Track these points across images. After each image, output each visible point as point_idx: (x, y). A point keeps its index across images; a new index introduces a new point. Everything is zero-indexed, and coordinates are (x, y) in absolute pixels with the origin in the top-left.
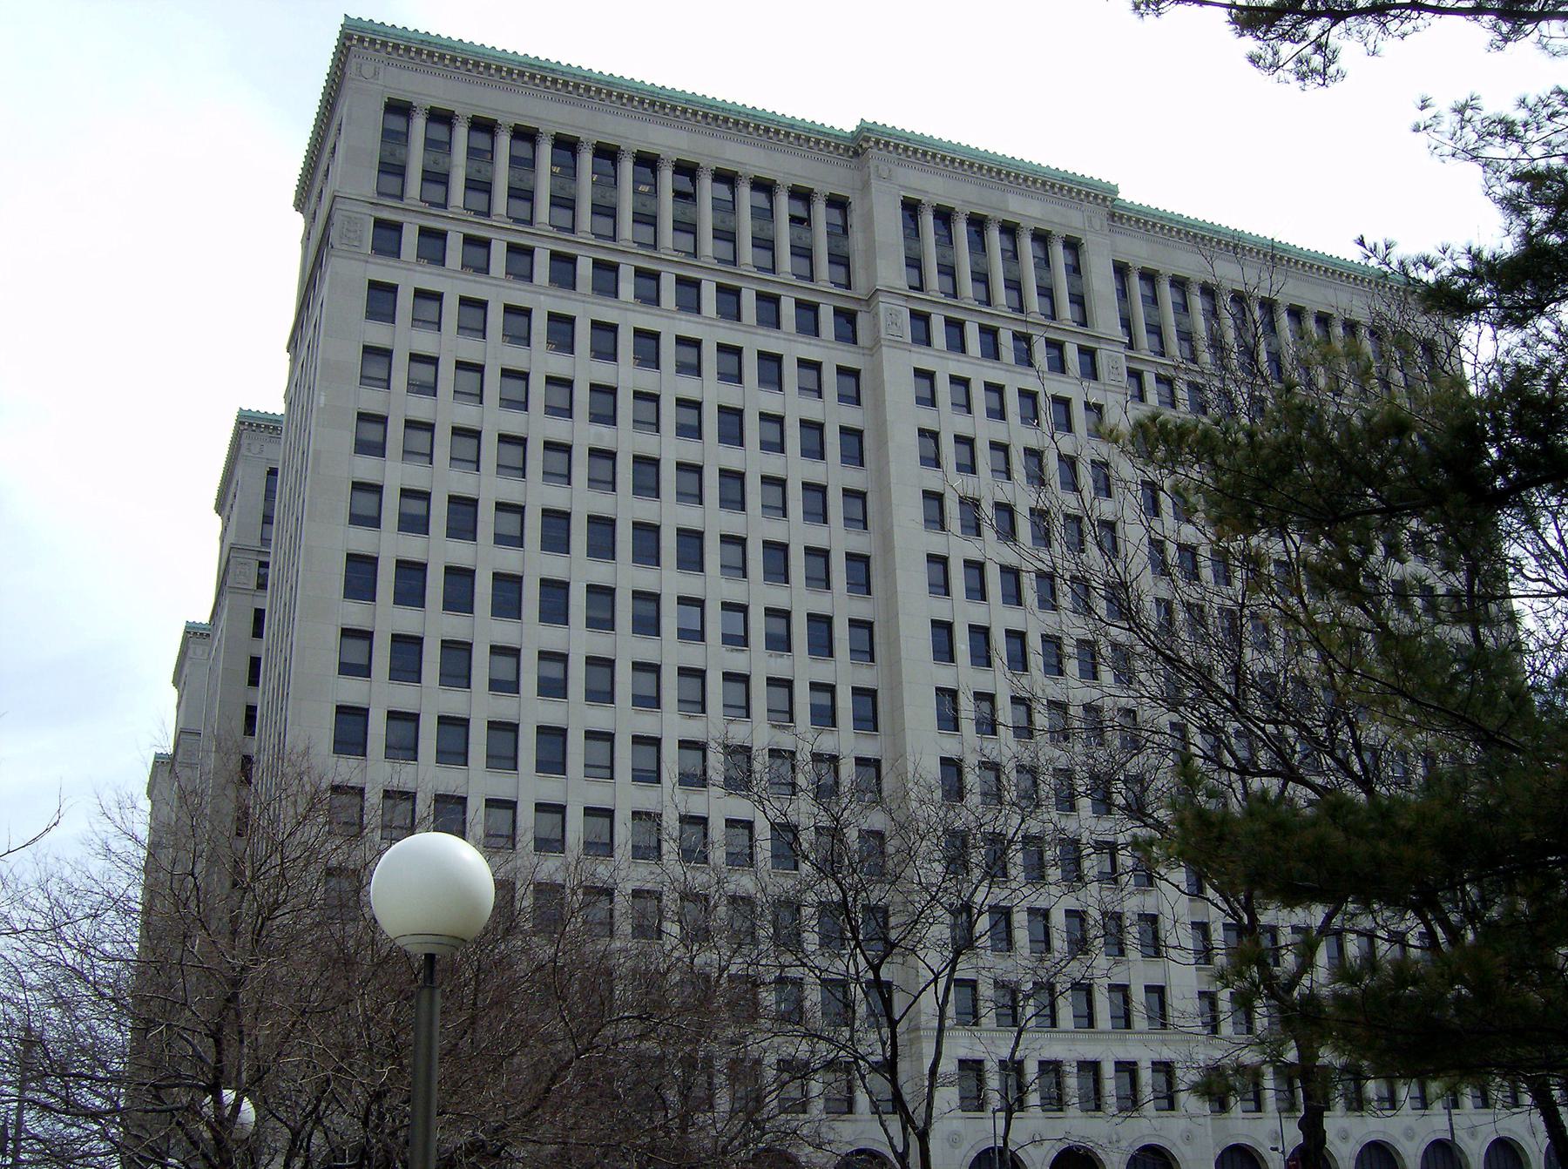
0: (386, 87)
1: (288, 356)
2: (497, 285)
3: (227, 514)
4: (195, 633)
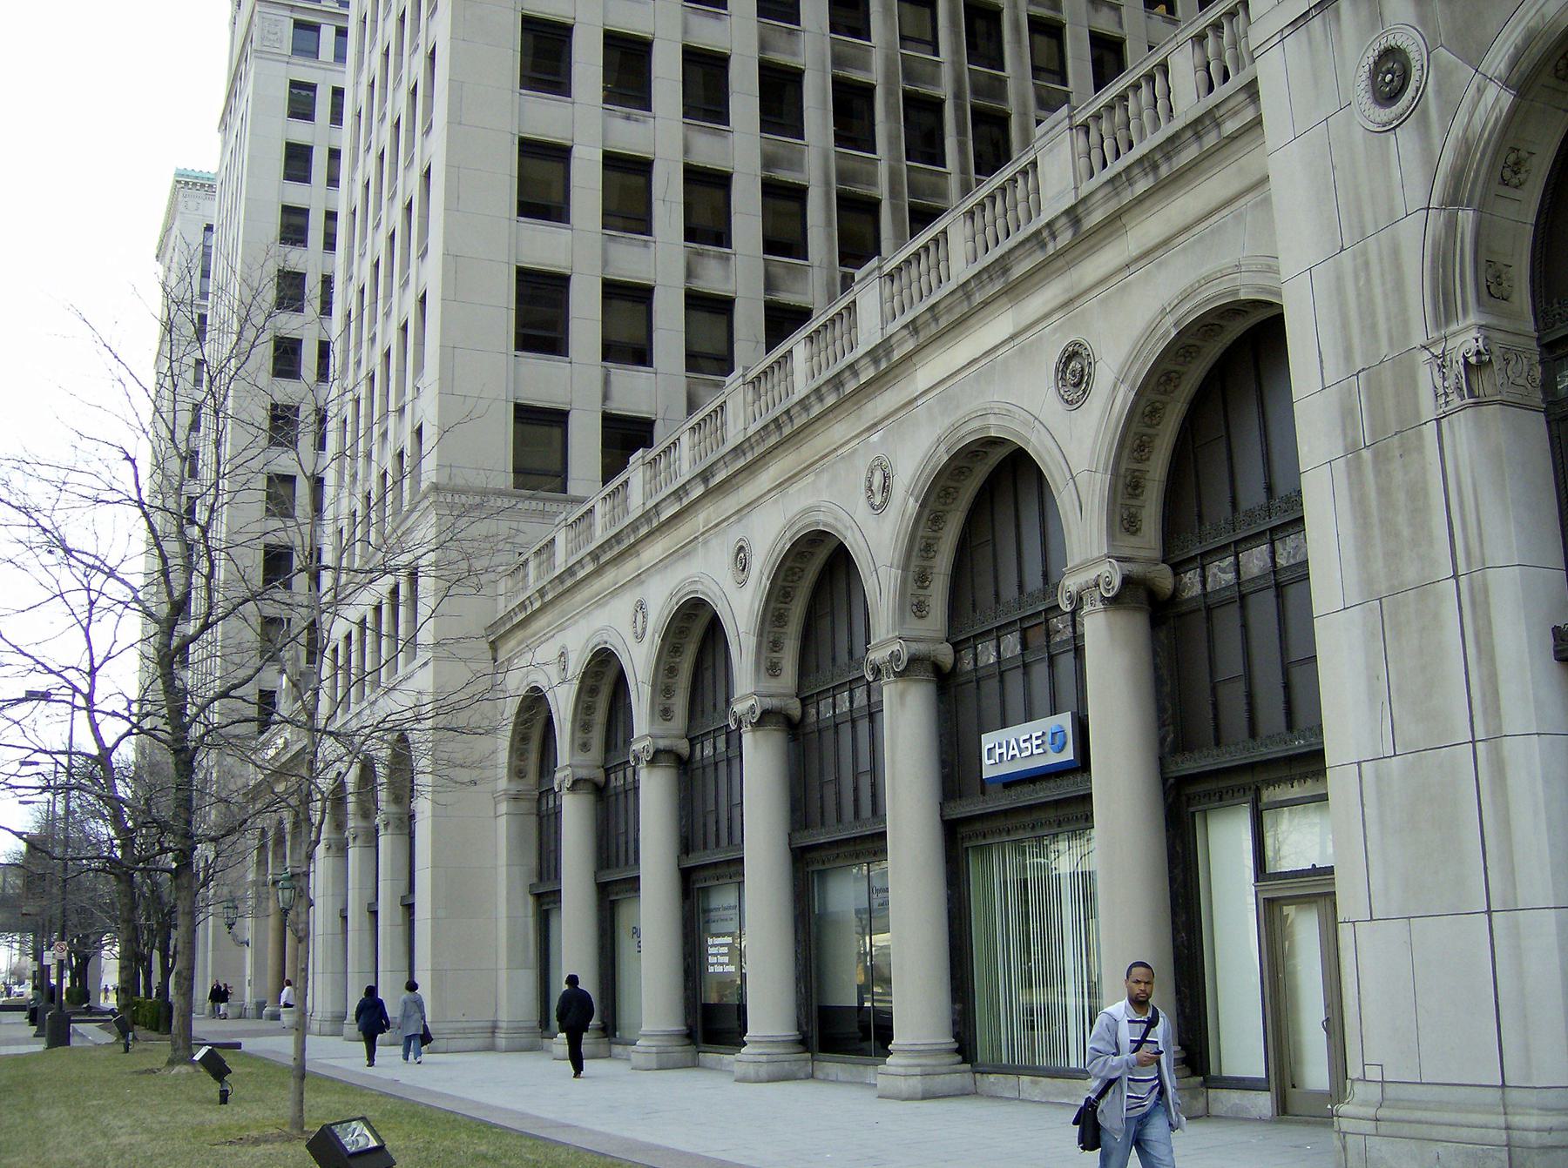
4: (187, 183)
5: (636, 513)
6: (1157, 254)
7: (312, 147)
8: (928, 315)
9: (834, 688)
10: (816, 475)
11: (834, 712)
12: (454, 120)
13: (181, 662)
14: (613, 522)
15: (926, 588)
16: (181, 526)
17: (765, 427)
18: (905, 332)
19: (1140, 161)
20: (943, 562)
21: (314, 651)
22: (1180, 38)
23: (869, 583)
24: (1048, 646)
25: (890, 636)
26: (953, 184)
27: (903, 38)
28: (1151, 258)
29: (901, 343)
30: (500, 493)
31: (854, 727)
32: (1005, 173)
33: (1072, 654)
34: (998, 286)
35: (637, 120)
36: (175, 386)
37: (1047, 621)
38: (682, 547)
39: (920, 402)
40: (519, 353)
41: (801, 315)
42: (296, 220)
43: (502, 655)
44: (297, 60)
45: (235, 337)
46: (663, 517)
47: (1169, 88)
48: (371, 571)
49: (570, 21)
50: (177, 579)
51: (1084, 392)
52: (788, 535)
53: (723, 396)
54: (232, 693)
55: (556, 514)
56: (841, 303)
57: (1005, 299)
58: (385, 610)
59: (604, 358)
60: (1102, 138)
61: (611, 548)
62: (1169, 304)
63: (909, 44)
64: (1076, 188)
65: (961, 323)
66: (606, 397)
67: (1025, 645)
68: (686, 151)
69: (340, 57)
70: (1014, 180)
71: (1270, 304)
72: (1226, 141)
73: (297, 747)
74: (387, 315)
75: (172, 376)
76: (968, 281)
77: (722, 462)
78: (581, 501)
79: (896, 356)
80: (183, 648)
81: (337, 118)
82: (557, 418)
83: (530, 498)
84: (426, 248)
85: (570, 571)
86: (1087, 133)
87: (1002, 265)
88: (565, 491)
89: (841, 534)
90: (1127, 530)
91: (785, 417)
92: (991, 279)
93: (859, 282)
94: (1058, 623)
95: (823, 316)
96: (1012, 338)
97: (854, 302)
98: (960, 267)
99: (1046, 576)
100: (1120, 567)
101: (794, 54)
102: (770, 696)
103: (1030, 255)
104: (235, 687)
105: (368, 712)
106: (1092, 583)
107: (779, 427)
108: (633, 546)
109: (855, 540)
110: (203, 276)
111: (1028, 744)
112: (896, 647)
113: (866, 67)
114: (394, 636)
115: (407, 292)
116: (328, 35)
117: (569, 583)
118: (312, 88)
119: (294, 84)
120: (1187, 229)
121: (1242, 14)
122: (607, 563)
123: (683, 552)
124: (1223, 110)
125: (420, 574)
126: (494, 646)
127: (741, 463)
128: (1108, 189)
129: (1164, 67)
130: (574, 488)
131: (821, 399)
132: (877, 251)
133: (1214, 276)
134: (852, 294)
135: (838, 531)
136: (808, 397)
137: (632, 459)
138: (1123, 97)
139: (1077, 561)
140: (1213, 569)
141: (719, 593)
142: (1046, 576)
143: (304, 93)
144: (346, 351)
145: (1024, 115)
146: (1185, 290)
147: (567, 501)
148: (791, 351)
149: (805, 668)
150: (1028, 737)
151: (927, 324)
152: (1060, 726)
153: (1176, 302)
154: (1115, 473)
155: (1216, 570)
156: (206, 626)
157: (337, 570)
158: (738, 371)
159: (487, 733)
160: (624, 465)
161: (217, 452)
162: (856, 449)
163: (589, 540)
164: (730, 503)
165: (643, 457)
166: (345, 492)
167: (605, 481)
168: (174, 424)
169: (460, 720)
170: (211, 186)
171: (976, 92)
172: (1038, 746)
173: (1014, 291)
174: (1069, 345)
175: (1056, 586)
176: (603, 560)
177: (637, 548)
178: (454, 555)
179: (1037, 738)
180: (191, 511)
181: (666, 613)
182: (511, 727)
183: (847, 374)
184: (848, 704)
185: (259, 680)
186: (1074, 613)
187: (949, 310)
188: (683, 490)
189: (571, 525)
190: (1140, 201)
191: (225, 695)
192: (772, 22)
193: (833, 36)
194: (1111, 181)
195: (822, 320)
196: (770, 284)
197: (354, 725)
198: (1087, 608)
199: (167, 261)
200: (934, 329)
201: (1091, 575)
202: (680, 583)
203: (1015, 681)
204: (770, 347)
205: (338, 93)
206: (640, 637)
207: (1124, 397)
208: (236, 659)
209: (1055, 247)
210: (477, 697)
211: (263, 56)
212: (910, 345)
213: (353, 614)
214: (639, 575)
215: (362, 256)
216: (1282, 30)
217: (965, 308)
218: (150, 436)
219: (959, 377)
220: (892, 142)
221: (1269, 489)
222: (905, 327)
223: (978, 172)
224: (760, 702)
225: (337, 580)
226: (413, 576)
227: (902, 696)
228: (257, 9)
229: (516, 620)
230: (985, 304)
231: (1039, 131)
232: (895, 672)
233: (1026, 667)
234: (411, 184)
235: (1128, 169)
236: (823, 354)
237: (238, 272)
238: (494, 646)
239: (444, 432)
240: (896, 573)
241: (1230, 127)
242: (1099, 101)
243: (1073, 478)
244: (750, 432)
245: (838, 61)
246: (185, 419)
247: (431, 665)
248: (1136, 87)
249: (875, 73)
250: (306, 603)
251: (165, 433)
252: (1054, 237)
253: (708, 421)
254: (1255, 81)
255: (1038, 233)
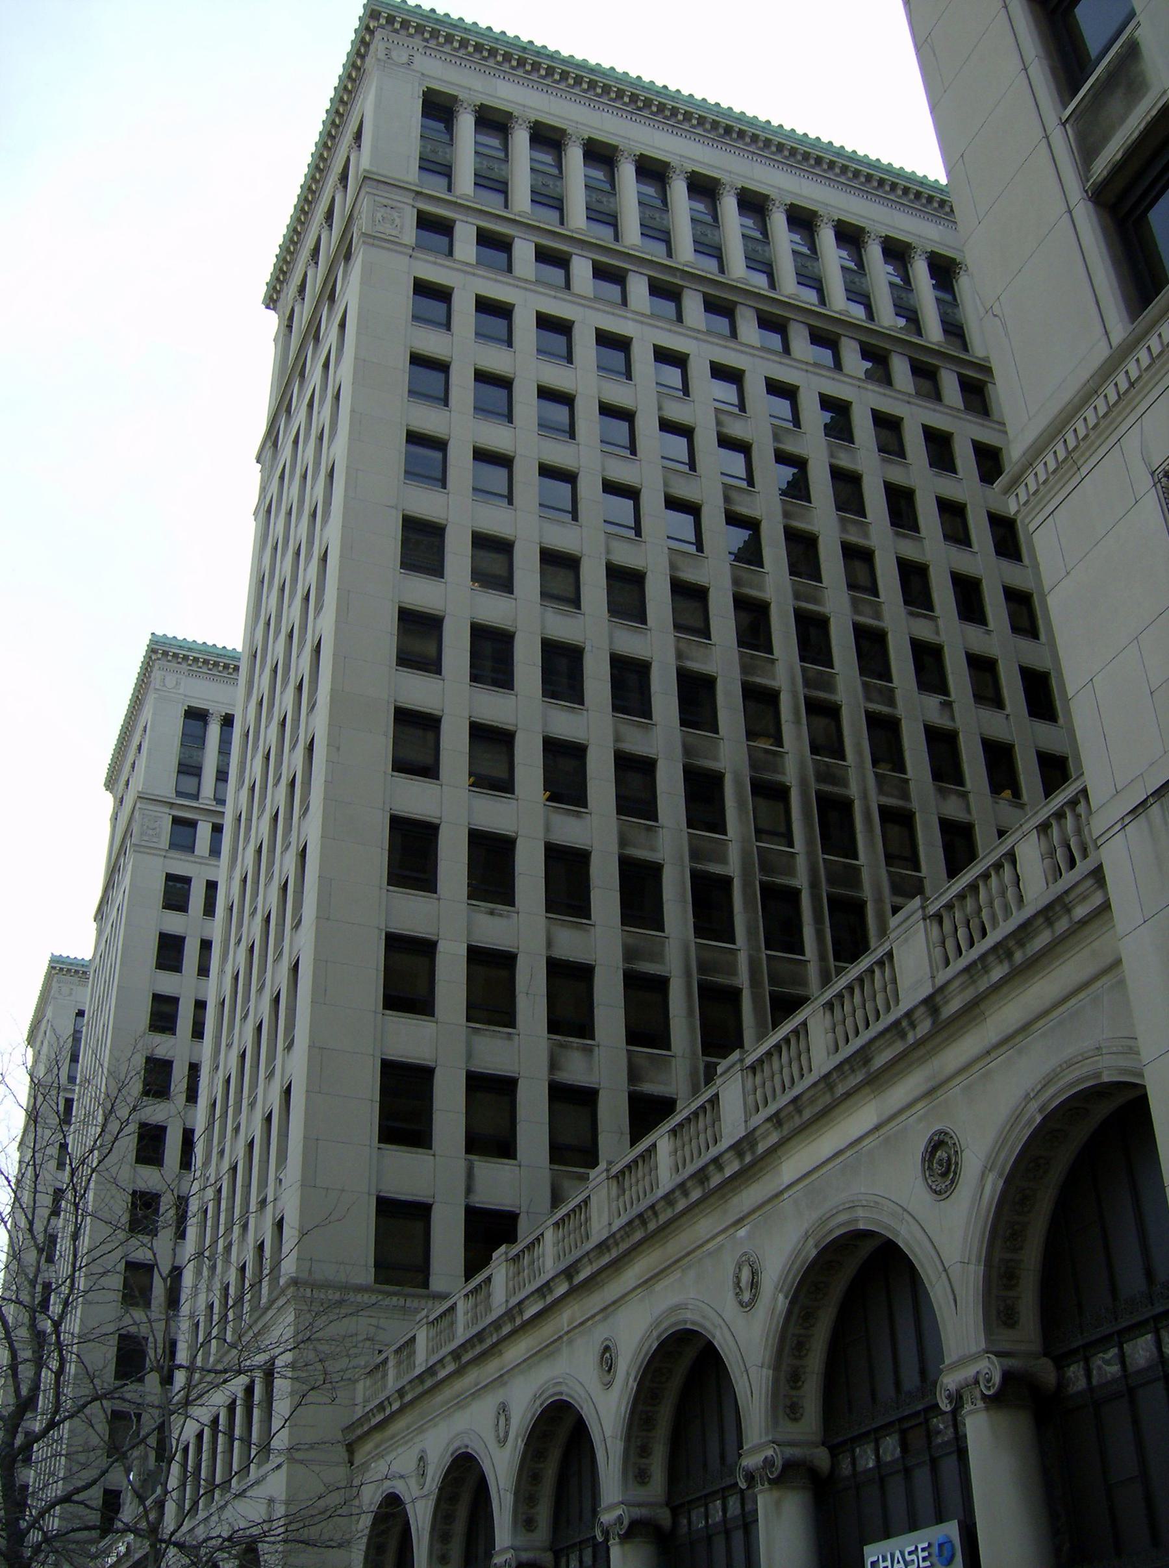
0: (185, 696)
1: (94, 925)
2: (526, 289)
3: (37, 1048)
4: (61, 969)
5: (498, 1309)
6: (1017, 1040)
7: (184, 938)
8: (791, 1108)
9: (706, 1496)
10: (683, 1270)
11: (707, 1522)
12: (323, 916)
13: (23, 1461)
14: (475, 1319)
15: (799, 1388)
16: (33, 1319)
17: (630, 1223)
18: (769, 1125)
19: (994, 949)
20: (815, 1362)
21: (163, 1454)
22: (1026, 827)
23: (740, 1385)
24: (929, 1448)
25: (763, 1440)
26: (813, 972)
27: (758, 831)
28: (1011, 1044)
29: (765, 1136)
30: (360, 1289)
31: (728, 1539)
32: (862, 965)
33: (954, 1457)
34: (859, 1077)
35: (501, 915)
36: (37, 1176)
37: (927, 1421)
38: (547, 1346)
39: (786, 1195)
40: (382, 1145)
41: (665, 1106)
42: (166, 1008)
43: (359, 1459)
44: (173, 854)
45: (99, 1130)
46: (527, 1316)
47: (1018, 876)
48: (225, 1371)
49: (437, 821)
50: (26, 1372)
51: (952, 1182)
52: (655, 1334)
53: (587, 1190)
54: (75, 1498)
55: (417, 1311)
56: (704, 1096)
57: (867, 1090)
58: (239, 1411)
59: (468, 1150)
60: (956, 927)
61: (473, 1347)
62: (1033, 1090)
63: (764, 836)
64: (933, 977)
65: (824, 1115)
66: (469, 1190)
67: (904, 1446)
68: (549, 944)
69: (215, 851)
70: (871, 971)
71: (1135, 1085)
72: (1077, 926)
73: (137, 1556)
74: (252, 1105)
75: (34, 1165)
76: (830, 1073)
77: (586, 1259)
78: (443, 1297)
79: (761, 1148)
80: (27, 1448)
81: (209, 909)
82: (420, 1212)
83: (395, 1294)
84: (293, 1040)
85: (431, 1371)
86: (941, 923)
87: (863, 1056)
88: (426, 1285)
89: (709, 1332)
90: (1005, 1323)
91: (650, 1213)
92: (853, 1071)
93: (721, 1075)
94: (939, 1423)
95: (686, 1110)
96: (877, 1128)
97: (717, 1095)
98: (822, 1060)
99: (923, 1373)
100: (1001, 1364)
101: (653, 849)
102: (639, 1505)
103: (890, 1045)
104: (78, 1491)
105: (215, 1518)
106: (971, 1380)
107: (644, 1223)
108: (494, 1345)
109: (725, 1339)
110: (71, 1061)
111: (914, 1557)
112: (770, 1452)
113: (723, 860)
114: (247, 1441)
115: (272, 1083)
116: (204, 831)
117: (429, 1383)
118: (187, 881)
119: (170, 877)
120: (1045, 1013)
121: (1083, 802)
122: (469, 1363)
123: (547, 1351)
124: (1072, 895)
125: (276, 1375)
126: (351, 1448)
127: (606, 1259)
128: (964, 977)
129: (1011, 856)
130: (437, 1283)
131: (686, 1194)
132: (740, 1045)
133: (1075, 1060)
134: (714, 1088)
135: (705, 1329)
136: (672, 1191)
137: (495, 1255)
138: (973, 888)
139: (954, 1358)
140: (1097, 1361)
141: (582, 1392)
142: (923, 1373)
143: (179, 885)
144: (210, 1141)
145: (879, 900)
146: (1048, 1075)
147: (428, 1296)
148: (654, 1145)
149: (673, 1477)
150: (913, 1548)
151: (790, 1117)
152: (947, 1537)
153: (1039, 1087)
154: (989, 1264)
155: (1100, 1362)
156: (52, 1425)
157: (191, 1369)
158: (603, 1165)
159: (340, 1546)
160: (486, 1261)
161: (74, 1244)
162: (723, 1245)
163: (452, 1337)
164: (596, 1301)
165: (506, 1253)
166: (203, 1286)
167: (468, 1276)
168: (33, 1214)
169: (312, 1533)
170: (84, 973)
171: (831, 881)
172: (924, 1559)
173: (877, 1081)
174: (934, 1134)
175: (935, 1384)
176: (466, 1358)
177: (500, 1347)
178: (311, 1356)
179: (923, 1550)
180: (45, 1305)
181: (529, 1416)
182: (365, 1540)
183: (712, 1168)
184: (720, 1513)
185: (104, 1482)
186: (955, 1412)
187: (812, 1101)
188: (546, 1288)
189: (433, 1322)
190: (997, 988)
191: (66, 1499)
192: (630, 819)
193: (691, 831)
194: (967, 969)
195: (685, 1114)
196: (634, 1075)
197: (201, 1533)
198: (968, 1407)
199: (38, 1044)
200: (797, 1121)
201: (969, 1372)
202: (546, 1383)
203: (896, 1488)
204: (634, 1141)
205: (212, 886)
206: (502, 1441)
207: (993, 1186)
208: (82, 1458)
209: (915, 1035)
210: (328, 1513)
211: (142, 850)
212: (774, 1138)
213: (202, 1413)
214: (501, 1376)
215: (229, 1046)
216: (1123, 818)
217: (827, 1099)
218: (9, 1224)
219: (824, 1170)
220: (751, 932)
221: (1149, 1275)
222: (768, 1120)
223: (837, 958)
224: (628, 1511)
225: (189, 1379)
226: (269, 1374)
227: (778, 1504)
228: (138, 805)
229: (374, 1422)
230: (848, 1095)
231: (893, 922)
232: (769, 1479)
233: (907, 1472)
234: (288, 864)
235: (983, 957)
236: (687, 1148)
237: (106, 1065)
238: (351, 1448)
239: (303, 1234)
240: (767, 1373)
241: (1080, 912)
242: (950, 891)
243: (945, 1270)
244: (615, 1228)
245: (695, 855)
246: (46, 1200)
247: (285, 1467)
248: (986, 876)
249: (733, 867)
250: (157, 1403)
251: (23, 1223)
252: (913, 1026)
253: (572, 1216)
254: (1100, 867)
255: (897, 1023)
